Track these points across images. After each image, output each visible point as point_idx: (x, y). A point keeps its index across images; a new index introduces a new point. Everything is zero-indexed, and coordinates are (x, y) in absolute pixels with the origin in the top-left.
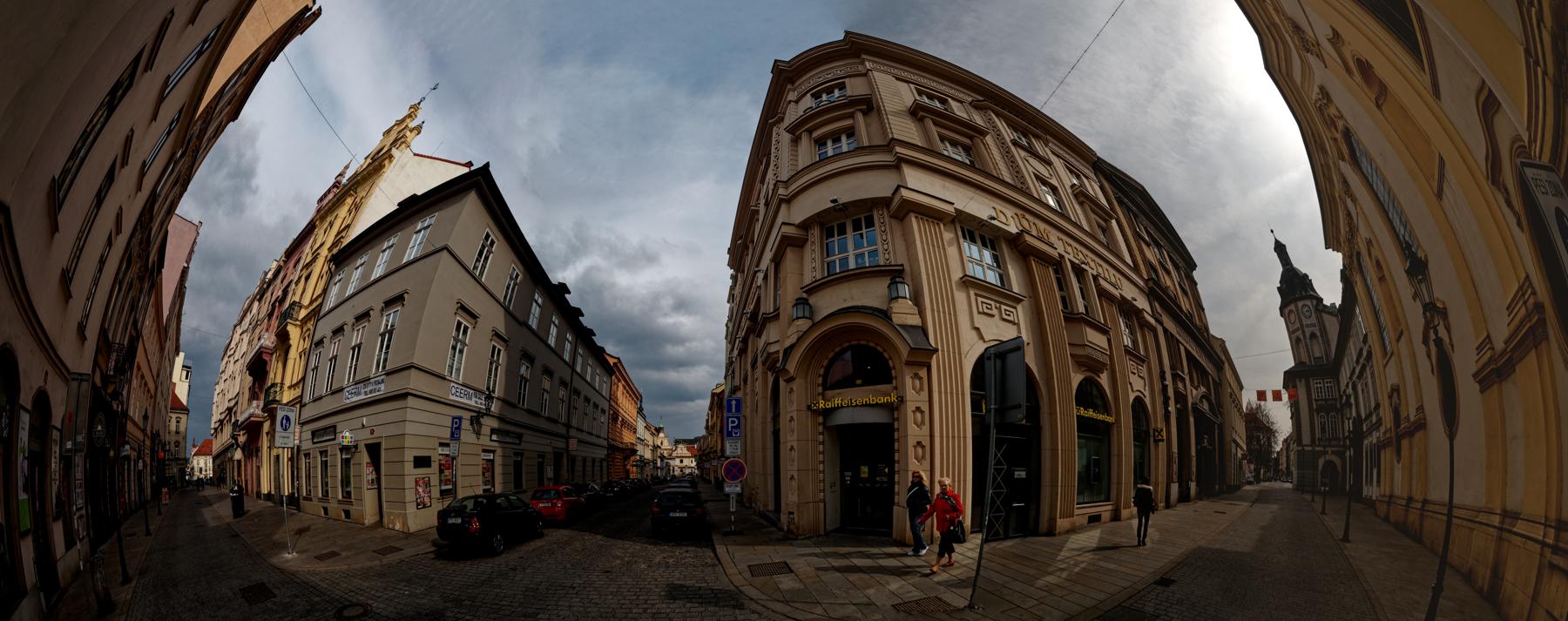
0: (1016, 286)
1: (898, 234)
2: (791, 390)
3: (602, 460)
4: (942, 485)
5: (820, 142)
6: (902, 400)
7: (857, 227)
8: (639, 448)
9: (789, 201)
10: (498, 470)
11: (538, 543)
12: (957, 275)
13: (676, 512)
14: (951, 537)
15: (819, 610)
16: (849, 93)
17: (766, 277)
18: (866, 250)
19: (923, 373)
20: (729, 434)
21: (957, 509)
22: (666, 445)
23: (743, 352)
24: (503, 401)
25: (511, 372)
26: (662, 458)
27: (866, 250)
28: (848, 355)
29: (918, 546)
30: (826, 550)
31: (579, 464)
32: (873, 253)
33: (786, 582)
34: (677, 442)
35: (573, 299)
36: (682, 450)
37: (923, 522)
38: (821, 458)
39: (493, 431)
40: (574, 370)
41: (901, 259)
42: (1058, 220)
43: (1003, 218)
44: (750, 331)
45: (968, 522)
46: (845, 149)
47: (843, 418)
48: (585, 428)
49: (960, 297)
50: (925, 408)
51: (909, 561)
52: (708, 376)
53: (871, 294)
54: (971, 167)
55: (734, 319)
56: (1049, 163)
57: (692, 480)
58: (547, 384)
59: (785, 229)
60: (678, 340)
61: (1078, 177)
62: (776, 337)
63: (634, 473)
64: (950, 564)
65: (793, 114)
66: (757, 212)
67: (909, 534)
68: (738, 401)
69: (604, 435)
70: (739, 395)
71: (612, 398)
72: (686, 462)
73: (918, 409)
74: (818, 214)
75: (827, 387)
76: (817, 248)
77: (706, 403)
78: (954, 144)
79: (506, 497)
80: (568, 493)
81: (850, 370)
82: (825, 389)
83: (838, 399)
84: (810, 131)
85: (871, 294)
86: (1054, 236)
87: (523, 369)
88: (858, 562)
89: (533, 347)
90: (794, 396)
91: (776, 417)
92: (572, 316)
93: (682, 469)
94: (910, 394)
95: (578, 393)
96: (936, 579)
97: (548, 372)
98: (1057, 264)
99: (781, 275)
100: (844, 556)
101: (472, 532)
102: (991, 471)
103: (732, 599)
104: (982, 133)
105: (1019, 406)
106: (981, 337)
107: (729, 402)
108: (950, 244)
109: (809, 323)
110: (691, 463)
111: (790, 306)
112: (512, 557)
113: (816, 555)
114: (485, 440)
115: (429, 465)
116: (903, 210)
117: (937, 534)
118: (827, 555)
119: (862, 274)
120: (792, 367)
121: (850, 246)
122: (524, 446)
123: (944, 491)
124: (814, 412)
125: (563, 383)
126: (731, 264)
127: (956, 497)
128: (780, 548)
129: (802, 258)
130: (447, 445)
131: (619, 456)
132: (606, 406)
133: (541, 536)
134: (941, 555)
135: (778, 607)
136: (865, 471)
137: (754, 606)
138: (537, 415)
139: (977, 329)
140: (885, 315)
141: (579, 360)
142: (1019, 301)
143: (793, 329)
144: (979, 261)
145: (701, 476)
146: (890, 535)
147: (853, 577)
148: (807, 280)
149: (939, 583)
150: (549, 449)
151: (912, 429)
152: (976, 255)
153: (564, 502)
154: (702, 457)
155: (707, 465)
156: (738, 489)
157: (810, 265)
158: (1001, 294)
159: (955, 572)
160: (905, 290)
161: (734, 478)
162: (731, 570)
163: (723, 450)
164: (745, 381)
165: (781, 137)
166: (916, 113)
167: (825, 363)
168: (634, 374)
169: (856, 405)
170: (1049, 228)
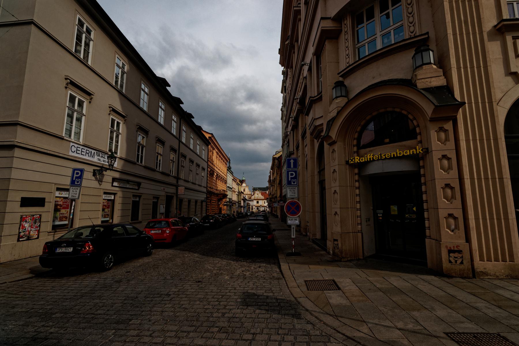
2: (334, 151)
3: (202, 202)
6: (427, 151)
8: (229, 193)
10: (118, 207)
11: (146, 260)
12: (490, 21)
13: (251, 239)
15: (365, 329)
17: (310, 70)
19: (449, 126)
22: (247, 191)
23: (295, 127)
24: (126, 160)
25: (130, 140)
26: (244, 200)
31: (185, 204)
33: (335, 298)
34: (255, 189)
35: (173, 90)
36: (258, 195)
38: (358, 199)
39: (114, 180)
40: (180, 141)
41: (427, 27)
44: (300, 112)
47: (374, 169)
48: (190, 179)
49: (494, 49)
50: (453, 155)
52: (270, 146)
53: (396, 68)
55: (287, 105)
57: (265, 215)
58: (160, 149)
60: (252, 121)
63: (225, 210)
69: (204, 184)
71: (209, 160)
72: (261, 203)
75: (359, 147)
77: (269, 165)
79: (123, 226)
80: (174, 224)
85: (396, 68)
87: (140, 139)
89: (146, 123)
90: (336, 155)
91: (321, 171)
92: (175, 104)
93: (258, 208)
95: (184, 157)
97: (160, 141)
101: (75, 257)
103: (290, 308)
109: (345, 100)
110: (264, 203)
112: (119, 272)
114: (107, 186)
115: (43, 205)
120: (333, 134)
121: (378, 29)
122: (141, 191)
124: (351, 165)
125: (173, 149)
126: (282, 63)
128: (330, 268)
130: (67, 190)
131: (214, 199)
132: (205, 165)
133: (149, 254)
135: (329, 320)
136: (394, 210)
137: (309, 317)
138: (153, 170)
140: (409, 84)
141: (184, 134)
143: (334, 106)
145: (271, 213)
148: (343, 66)
150: (163, 193)
153: (172, 230)
154: (271, 200)
155: (276, 205)
156: (297, 222)
157: (344, 54)
161: (294, 213)
162: (292, 284)
167: (359, 129)
168: (223, 144)
169: (386, 159)
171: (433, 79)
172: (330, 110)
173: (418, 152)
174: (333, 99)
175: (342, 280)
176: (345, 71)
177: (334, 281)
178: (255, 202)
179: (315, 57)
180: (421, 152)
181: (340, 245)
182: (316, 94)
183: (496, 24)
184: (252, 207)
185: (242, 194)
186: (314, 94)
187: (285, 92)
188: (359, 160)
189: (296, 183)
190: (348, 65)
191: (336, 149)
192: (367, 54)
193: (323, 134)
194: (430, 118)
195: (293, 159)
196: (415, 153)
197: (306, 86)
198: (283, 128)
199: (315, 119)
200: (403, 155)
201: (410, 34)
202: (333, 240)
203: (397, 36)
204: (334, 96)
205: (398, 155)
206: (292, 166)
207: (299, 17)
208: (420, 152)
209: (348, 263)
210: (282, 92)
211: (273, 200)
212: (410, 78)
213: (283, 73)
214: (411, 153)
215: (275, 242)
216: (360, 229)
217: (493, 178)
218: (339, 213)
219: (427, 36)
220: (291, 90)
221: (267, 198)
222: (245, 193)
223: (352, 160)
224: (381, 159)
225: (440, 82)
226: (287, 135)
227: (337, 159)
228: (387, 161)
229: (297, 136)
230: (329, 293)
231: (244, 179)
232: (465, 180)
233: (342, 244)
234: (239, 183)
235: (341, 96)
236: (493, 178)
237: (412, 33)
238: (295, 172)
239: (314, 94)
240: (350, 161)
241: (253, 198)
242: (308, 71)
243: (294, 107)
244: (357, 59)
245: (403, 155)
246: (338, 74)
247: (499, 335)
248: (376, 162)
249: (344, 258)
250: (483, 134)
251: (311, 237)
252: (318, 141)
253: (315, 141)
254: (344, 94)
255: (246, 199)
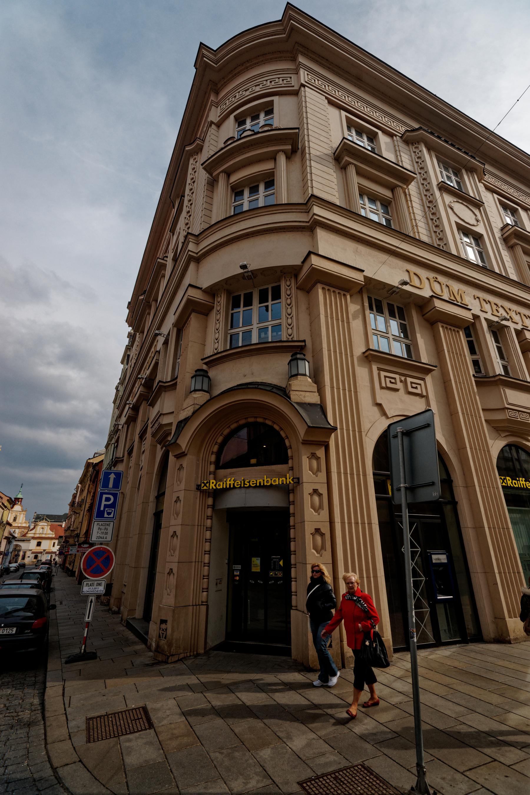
0: (425, 356)
1: (303, 307)
2: (181, 468)
4: (348, 582)
5: (237, 191)
6: (298, 481)
7: (263, 299)
9: (198, 259)
12: (359, 349)
14: (369, 662)
16: (276, 124)
17: (166, 343)
18: (269, 324)
19: (321, 453)
20: (100, 514)
21: (370, 616)
22: (22, 521)
23: (132, 420)
27: (269, 324)
28: (244, 433)
29: (326, 672)
30: (206, 678)
32: (277, 328)
33: (139, 749)
34: (38, 518)
37: (329, 633)
38: (207, 547)
41: (304, 334)
42: (482, 278)
43: (416, 282)
44: (142, 398)
45: (387, 635)
46: (261, 203)
47: (235, 501)
49: (362, 373)
50: (323, 490)
51: (317, 696)
52: (87, 442)
53: (269, 370)
54: (387, 228)
55: (126, 382)
56: (476, 204)
59: (192, 292)
60: (58, 394)
61: (514, 212)
62: (170, 408)
64: (374, 703)
65: (215, 142)
66: (164, 266)
67: (312, 652)
68: (118, 475)
70: (120, 468)
72: (46, 545)
73: (315, 491)
74: (227, 281)
75: (218, 466)
76: (222, 317)
77: (78, 473)
78: (373, 198)
81: (245, 448)
82: (218, 467)
83: (230, 478)
84: (228, 174)
85: (269, 370)
86: (469, 296)
88: (249, 698)
90: (184, 474)
91: (160, 496)
94: (307, 475)
96: (359, 729)
98: (470, 328)
99: (183, 343)
100: (230, 688)
102: (409, 565)
104: (405, 179)
105: (433, 484)
106: (384, 413)
107: (107, 475)
108: (355, 317)
109: (207, 396)
110: (51, 547)
111: (188, 376)
113: (190, 688)
116: (310, 279)
117: (349, 652)
118: (205, 687)
119: (264, 349)
120: (184, 442)
121: (255, 319)
123: (351, 591)
124: (203, 492)
126: (130, 321)
127: (367, 599)
129: (205, 328)
134: (358, 687)
139: (379, 405)
140: (283, 392)
142: (427, 371)
143: (189, 401)
144: (385, 333)
146: (287, 652)
147: (242, 726)
148: (209, 352)
149: (363, 737)
151: (309, 514)
152: (382, 327)
154: (67, 541)
155: (73, 551)
156: (101, 589)
158: (409, 367)
159: (384, 717)
160: (305, 367)
161: (97, 572)
163: (88, 533)
164: (130, 453)
165: (197, 175)
166: (344, 157)
167: (220, 439)
170: (463, 287)
171: (308, 394)
172: (185, 406)
173: (288, 483)
174: (191, 392)
175: (158, 705)
176: (211, 358)
177: (145, 709)
178: (34, 543)
179: (175, 329)
180: (292, 482)
181: (169, 631)
182: (169, 379)
183: (364, 351)
184: (25, 553)
185: (8, 527)
186: (166, 379)
187: (127, 364)
188: (215, 485)
189: (112, 516)
190: (216, 351)
191: (184, 465)
192: (240, 345)
193: (169, 438)
194: (303, 440)
195: (114, 473)
196: (285, 483)
197: (157, 364)
198: (113, 417)
199: (161, 414)
200: (271, 484)
201: (288, 336)
202: (159, 622)
203: (275, 334)
204: (192, 389)
205: (265, 484)
206: (111, 485)
207: (163, 272)
208: (290, 483)
209: (178, 666)
210: (122, 362)
211: (71, 541)
212: (284, 386)
213: (130, 335)
214: (281, 483)
215: (51, 631)
216: (204, 600)
217: (363, 523)
218: (175, 571)
219: (303, 344)
220: (135, 364)
221: (61, 537)
222: (14, 524)
223: (205, 485)
224: (244, 487)
225: (314, 398)
226: (118, 430)
227: (184, 480)
228: (251, 490)
229: (133, 434)
230: (129, 741)
231: (20, 496)
232: (336, 524)
233: (173, 628)
234: (6, 504)
235: (202, 390)
236: (363, 523)
237: (290, 336)
238: (115, 495)
239: (166, 379)
240: (203, 485)
241: (30, 535)
242: (164, 344)
243: (135, 389)
244: (228, 348)
245: (271, 484)
246: (202, 360)
247: (363, 766)
248: (237, 491)
249: (173, 655)
250: (353, 468)
251: (125, 615)
252: (162, 448)
253: (159, 446)
254: (205, 387)
255: (14, 537)
